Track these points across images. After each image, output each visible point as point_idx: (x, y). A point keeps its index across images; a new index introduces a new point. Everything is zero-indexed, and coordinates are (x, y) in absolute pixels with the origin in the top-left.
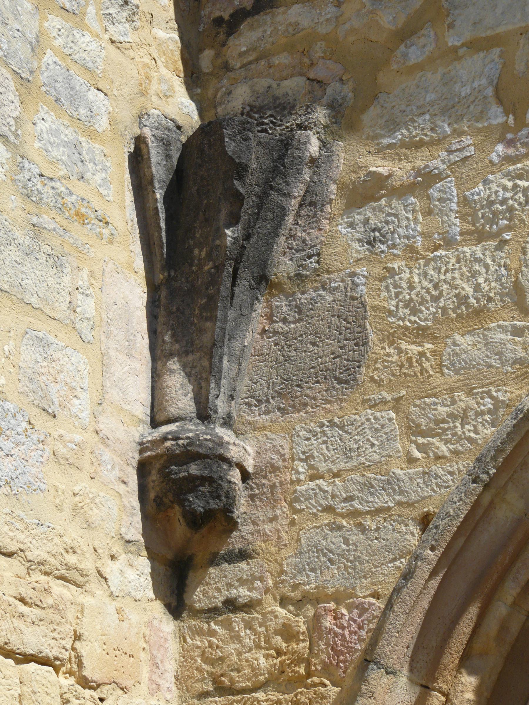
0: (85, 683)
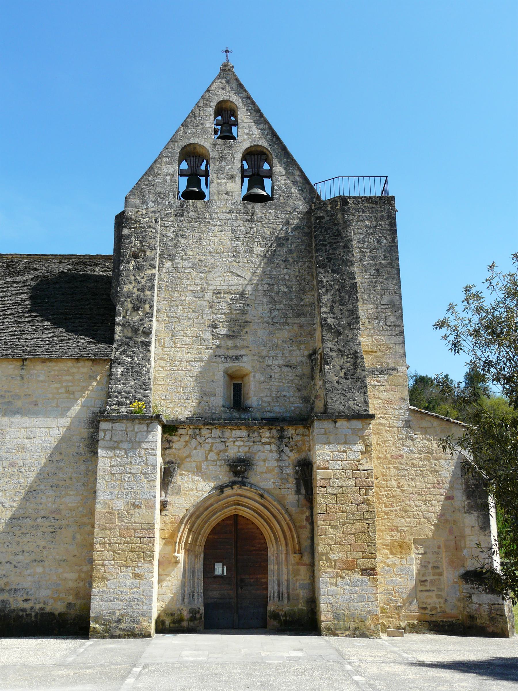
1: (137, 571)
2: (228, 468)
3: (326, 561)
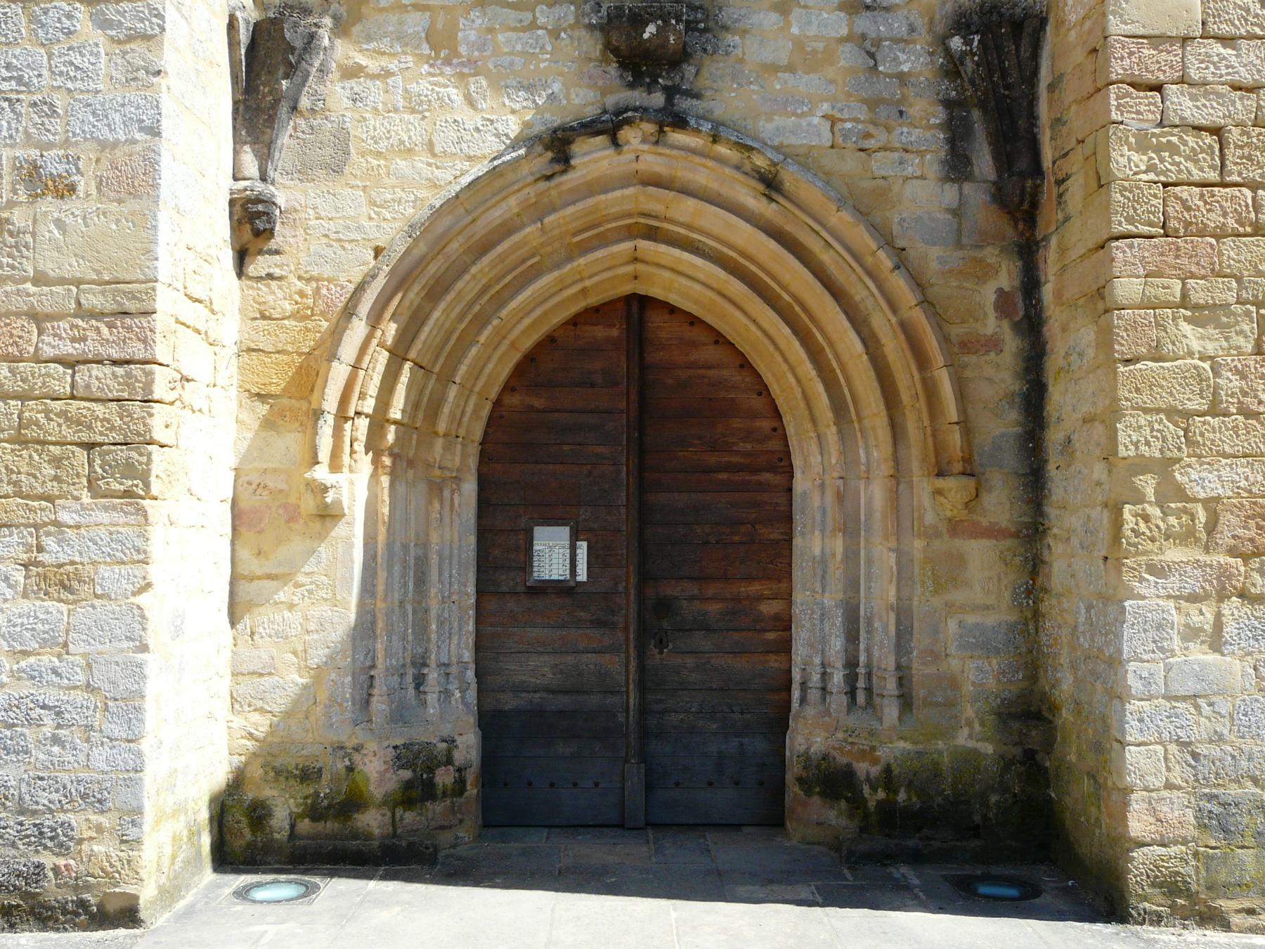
0: (213, 311)
1: (54, 552)
2: (592, 45)
3: (1160, 504)
